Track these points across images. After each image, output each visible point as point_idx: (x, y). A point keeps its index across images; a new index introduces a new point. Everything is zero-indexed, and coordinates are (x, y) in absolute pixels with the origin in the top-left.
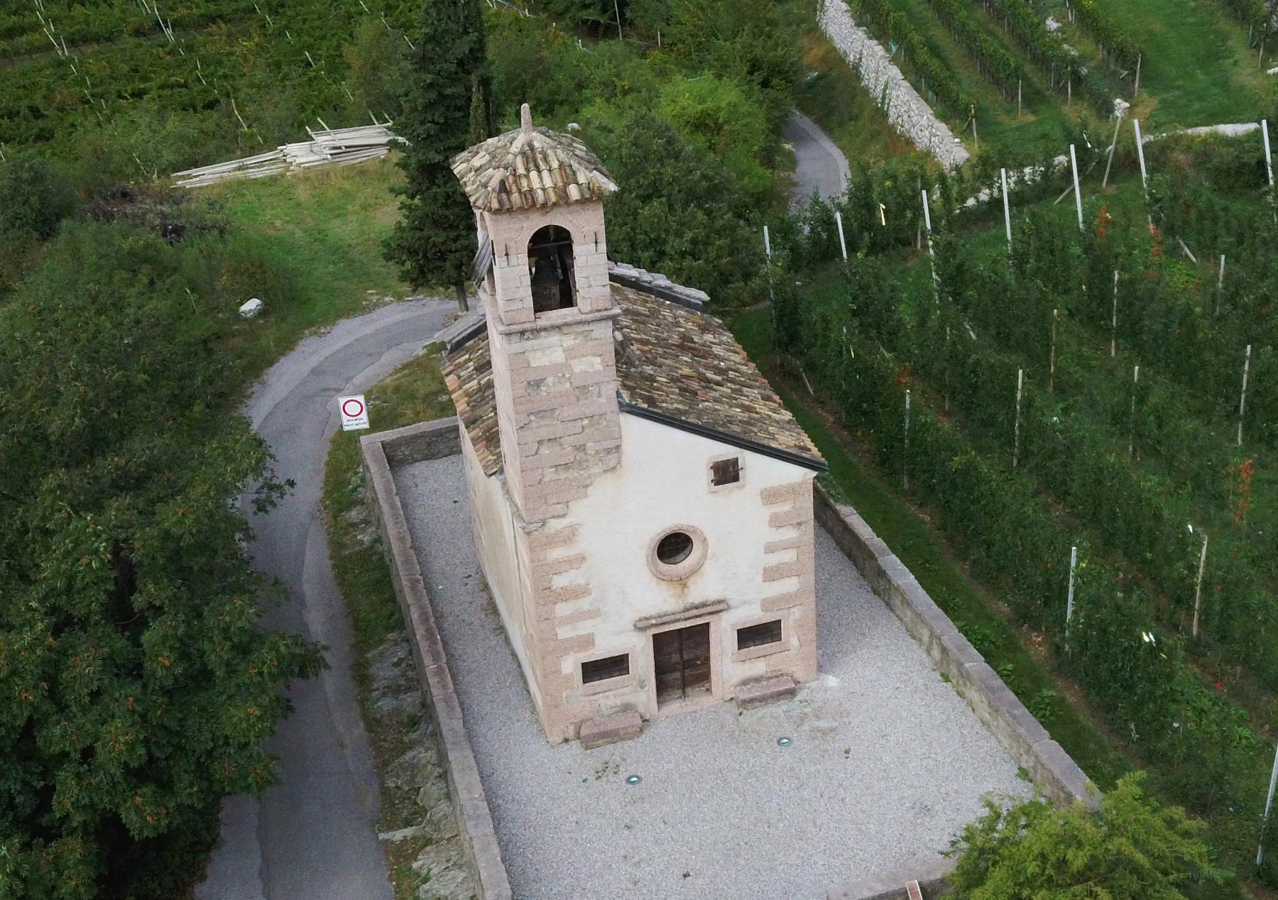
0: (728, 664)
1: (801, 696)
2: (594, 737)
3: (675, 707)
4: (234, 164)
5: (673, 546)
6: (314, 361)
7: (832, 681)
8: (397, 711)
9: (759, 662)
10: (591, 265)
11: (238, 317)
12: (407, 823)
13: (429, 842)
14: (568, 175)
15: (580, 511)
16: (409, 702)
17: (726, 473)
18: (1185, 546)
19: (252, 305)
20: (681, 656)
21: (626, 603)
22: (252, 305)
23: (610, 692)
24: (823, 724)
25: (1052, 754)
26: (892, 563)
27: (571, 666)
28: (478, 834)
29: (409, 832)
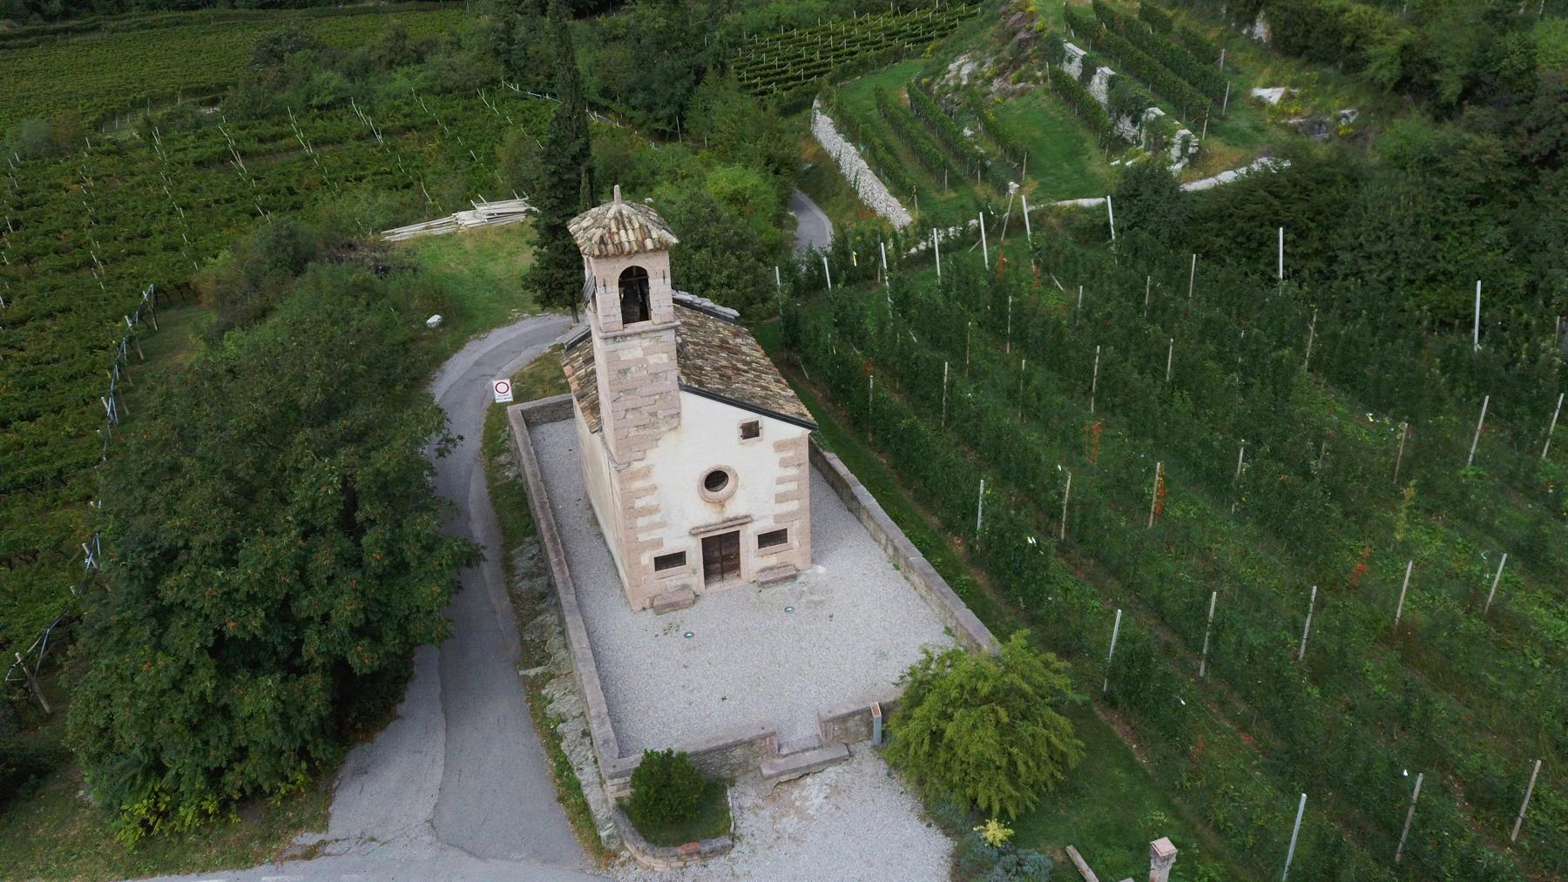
0: (752, 558)
1: (801, 579)
2: (663, 606)
3: (716, 586)
4: (423, 225)
5: (715, 479)
6: (476, 357)
7: (821, 569)
8: (532, 589)
9: (772, 557)
10: (660, 292)
11: (425, 327)
12: (538, 664)
13: (553, 676)
14: (646, 233)
15: (653, 456)
16: (539, 583)
17: (750, 431)
18: (1056, 479)
19: (435, 319)
20: (720, 553)
21: (684, 518)
22: (435, 319)
23: (673, 578)
24: (815, 598)
26: (861, 491)
27: (647, 559)
28: (585, 670)
29: (539, 670)
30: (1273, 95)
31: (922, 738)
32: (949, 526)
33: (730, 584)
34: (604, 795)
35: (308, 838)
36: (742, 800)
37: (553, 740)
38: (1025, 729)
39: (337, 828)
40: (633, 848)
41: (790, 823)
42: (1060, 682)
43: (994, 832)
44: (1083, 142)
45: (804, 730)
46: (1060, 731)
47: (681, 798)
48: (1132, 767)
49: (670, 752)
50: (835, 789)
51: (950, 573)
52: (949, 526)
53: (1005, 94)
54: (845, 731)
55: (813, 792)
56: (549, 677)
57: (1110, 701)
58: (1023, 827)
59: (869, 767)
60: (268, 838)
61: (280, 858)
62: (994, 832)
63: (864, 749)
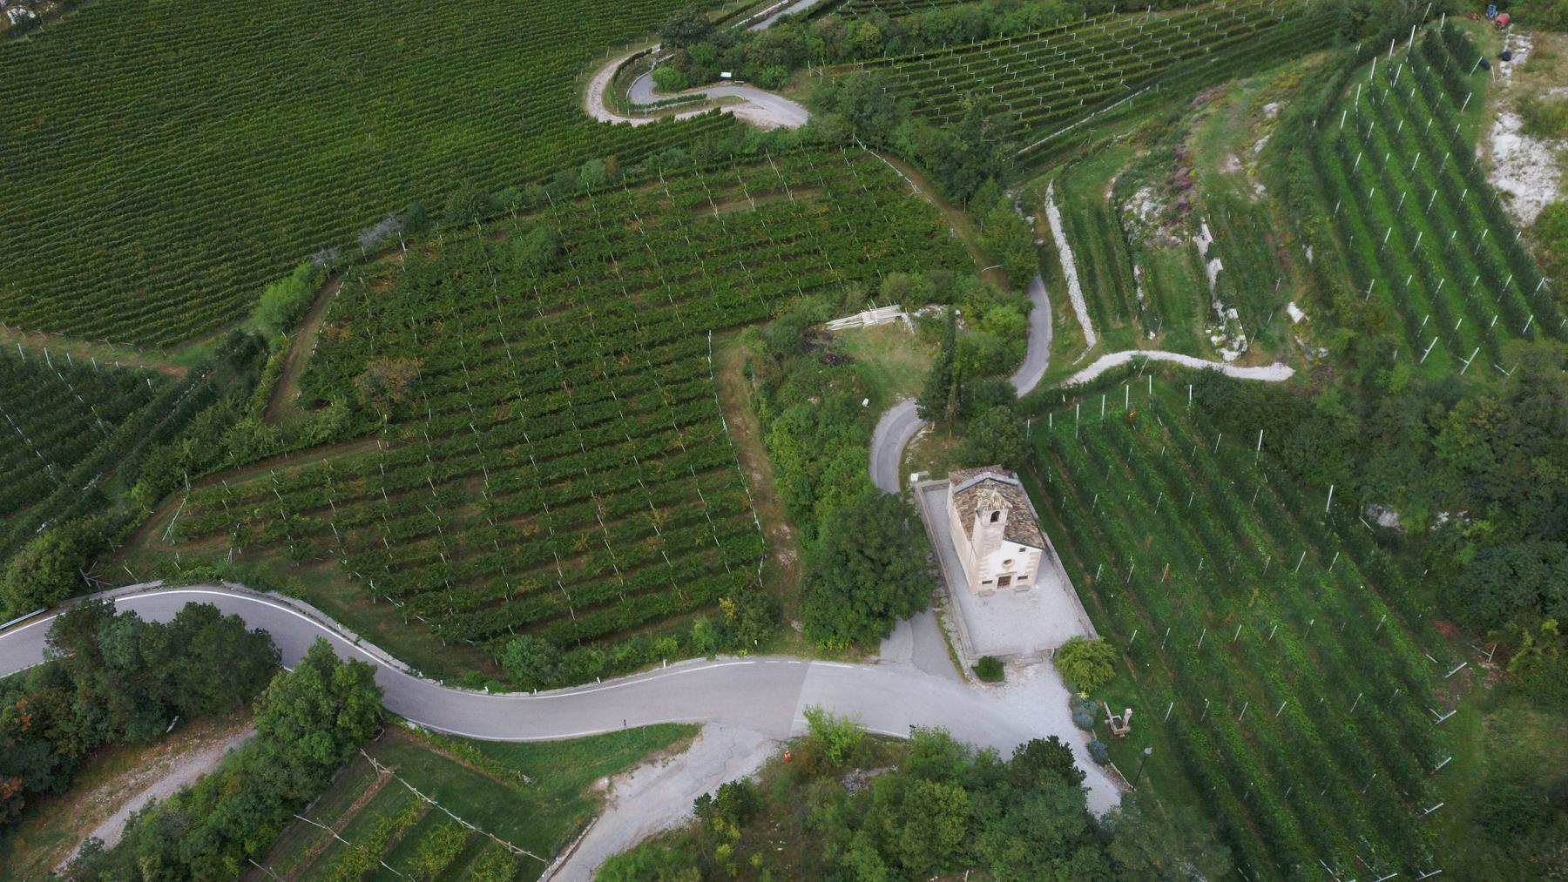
0: (1014, 583)
2: (981, 594)
5: (1007, 562)
9: (1022, 583)
10: (1003, 517)
16: (935, 572)
19: (866, 402)
20: (1004, 581)
21: (994, 570)
22: (866, 402)
25: (1092, 630)
26: (1055, 554)
28: (958, 609)
30: (1295, 313)
31: (1066, 659)
32: (1086, 569)
33: (1006, 589)
34: (968, 663)
35: (874, 658)
36: (1008, 670)
37: (947, 639)
38: (1098, 669)
39: (882, 657)
40: (974, 680)
41: (1022, 680)
42: (1111, 654)
43: (1083, 695)
44: (1196, 305)
45: (1028, 651)
46: (1109, 671)
47: (990, 670)
48: (1130, 678)
49: (1054, 739)
50: (1037, 672)
51: (1081, 594)
52: (1086, 569)
53: (1164, 243)
54: (1040, 655)
55: (1030, 671)
56: (942, 613)
57: (1128, 654)
58: (1092, 695)
59: (1049, 666)
60: (863, 655)
61: (867, 663)
62: (1083, 695)
63: (1047, 660)
